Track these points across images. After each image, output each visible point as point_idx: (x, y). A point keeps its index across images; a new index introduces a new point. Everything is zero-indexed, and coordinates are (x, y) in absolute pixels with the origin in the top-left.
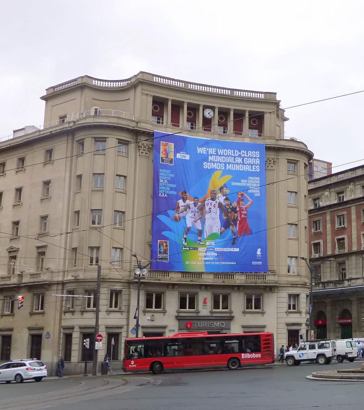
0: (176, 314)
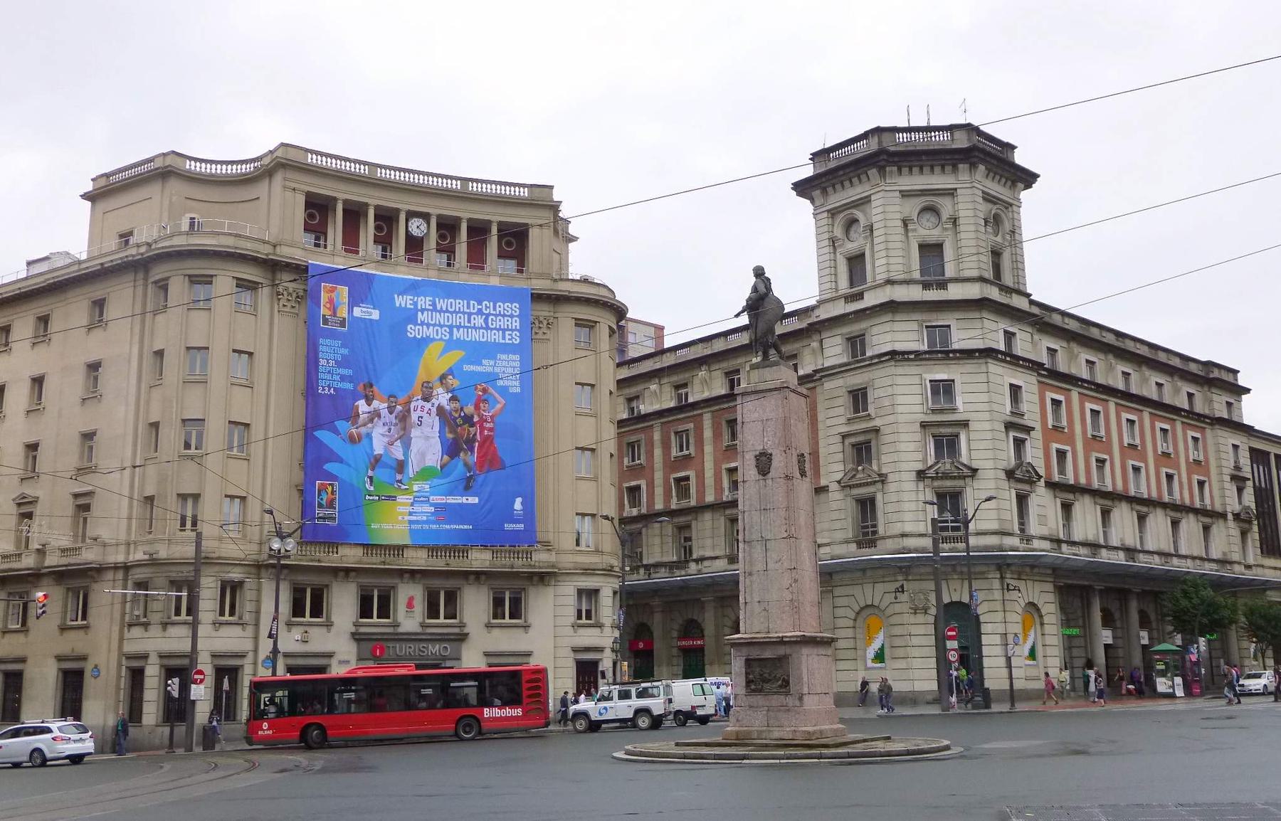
0: (353, 629)
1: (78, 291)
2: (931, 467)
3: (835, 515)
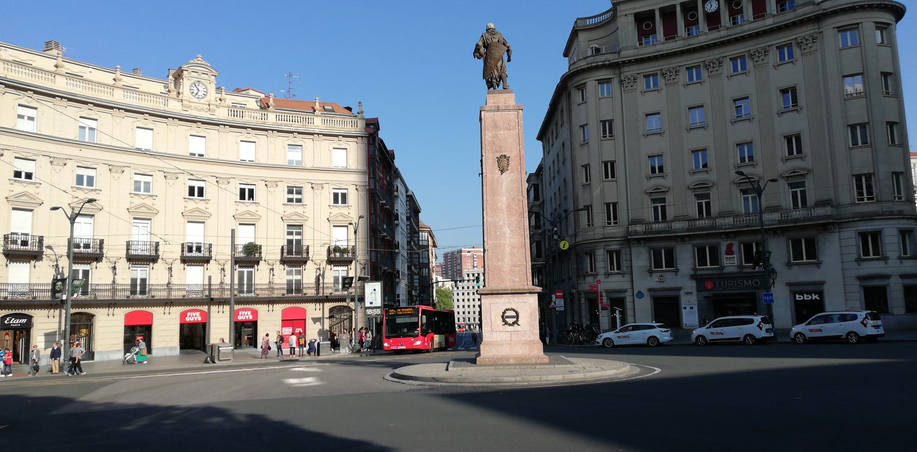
0: (692, 273)
1: (572, 106)
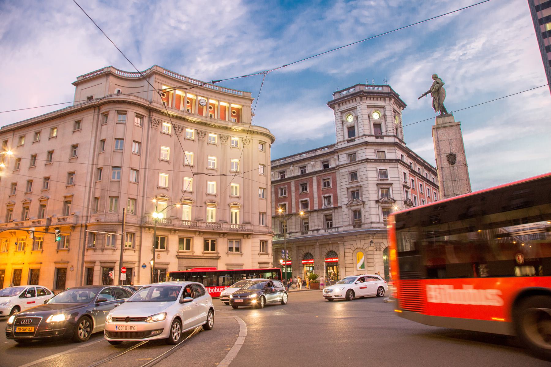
0: (177, 254)
1: (70, 118)
2: (381, 199)
3: (344, 217)
